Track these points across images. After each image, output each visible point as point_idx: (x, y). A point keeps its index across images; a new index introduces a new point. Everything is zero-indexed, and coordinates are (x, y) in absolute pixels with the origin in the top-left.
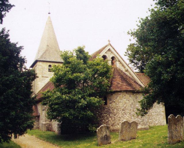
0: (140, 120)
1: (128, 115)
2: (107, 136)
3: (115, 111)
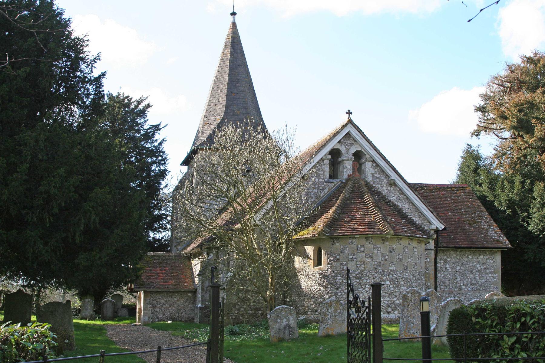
0: (397, 302)
1: (367, 289)
2: (290, 327)
3: (337, 280)
